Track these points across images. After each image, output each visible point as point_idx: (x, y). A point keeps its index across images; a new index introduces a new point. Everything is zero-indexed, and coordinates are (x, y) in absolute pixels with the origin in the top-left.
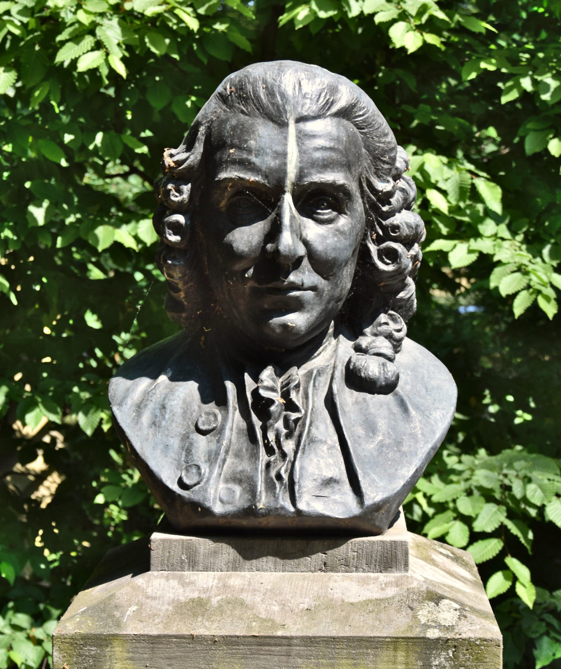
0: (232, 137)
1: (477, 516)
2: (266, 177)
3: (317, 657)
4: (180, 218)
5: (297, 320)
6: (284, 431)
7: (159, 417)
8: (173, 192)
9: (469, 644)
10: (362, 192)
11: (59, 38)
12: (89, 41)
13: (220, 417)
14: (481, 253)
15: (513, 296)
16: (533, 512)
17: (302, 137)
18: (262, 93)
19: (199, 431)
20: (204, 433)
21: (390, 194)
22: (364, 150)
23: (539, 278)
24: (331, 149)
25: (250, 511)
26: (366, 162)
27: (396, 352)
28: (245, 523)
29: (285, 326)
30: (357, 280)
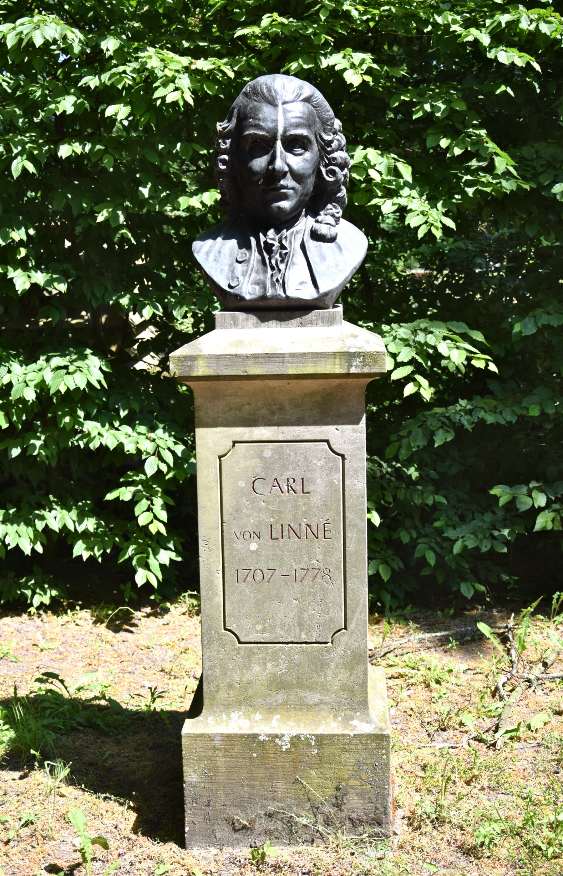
0: (251, 113)
1: (399, 353)
2: (268, 132)
3: (297, 363)
4: (226, 157)
5: (285, 204)
6: (280, 259)
7: (217, 257)
8: (222, 143)
9: (371, 355)
10: (317, 141)
11: (154, 85)
12: (171, 86)
13: (248, 255)
14: (400, 205)
15: (419, 227)
16: (431, 351)
17: (285, 111)
18: (265, 91)
19: (237, 261)
20: (240, 262)
21: (331, 142)
22: (317, 119)
23: (433, 217)
24: (300, 117)
25: (263, 297)
26: (319, 125)
27: (337, 224)
28: (261, 304)
29: (279, 208)
30: (316, 186)
